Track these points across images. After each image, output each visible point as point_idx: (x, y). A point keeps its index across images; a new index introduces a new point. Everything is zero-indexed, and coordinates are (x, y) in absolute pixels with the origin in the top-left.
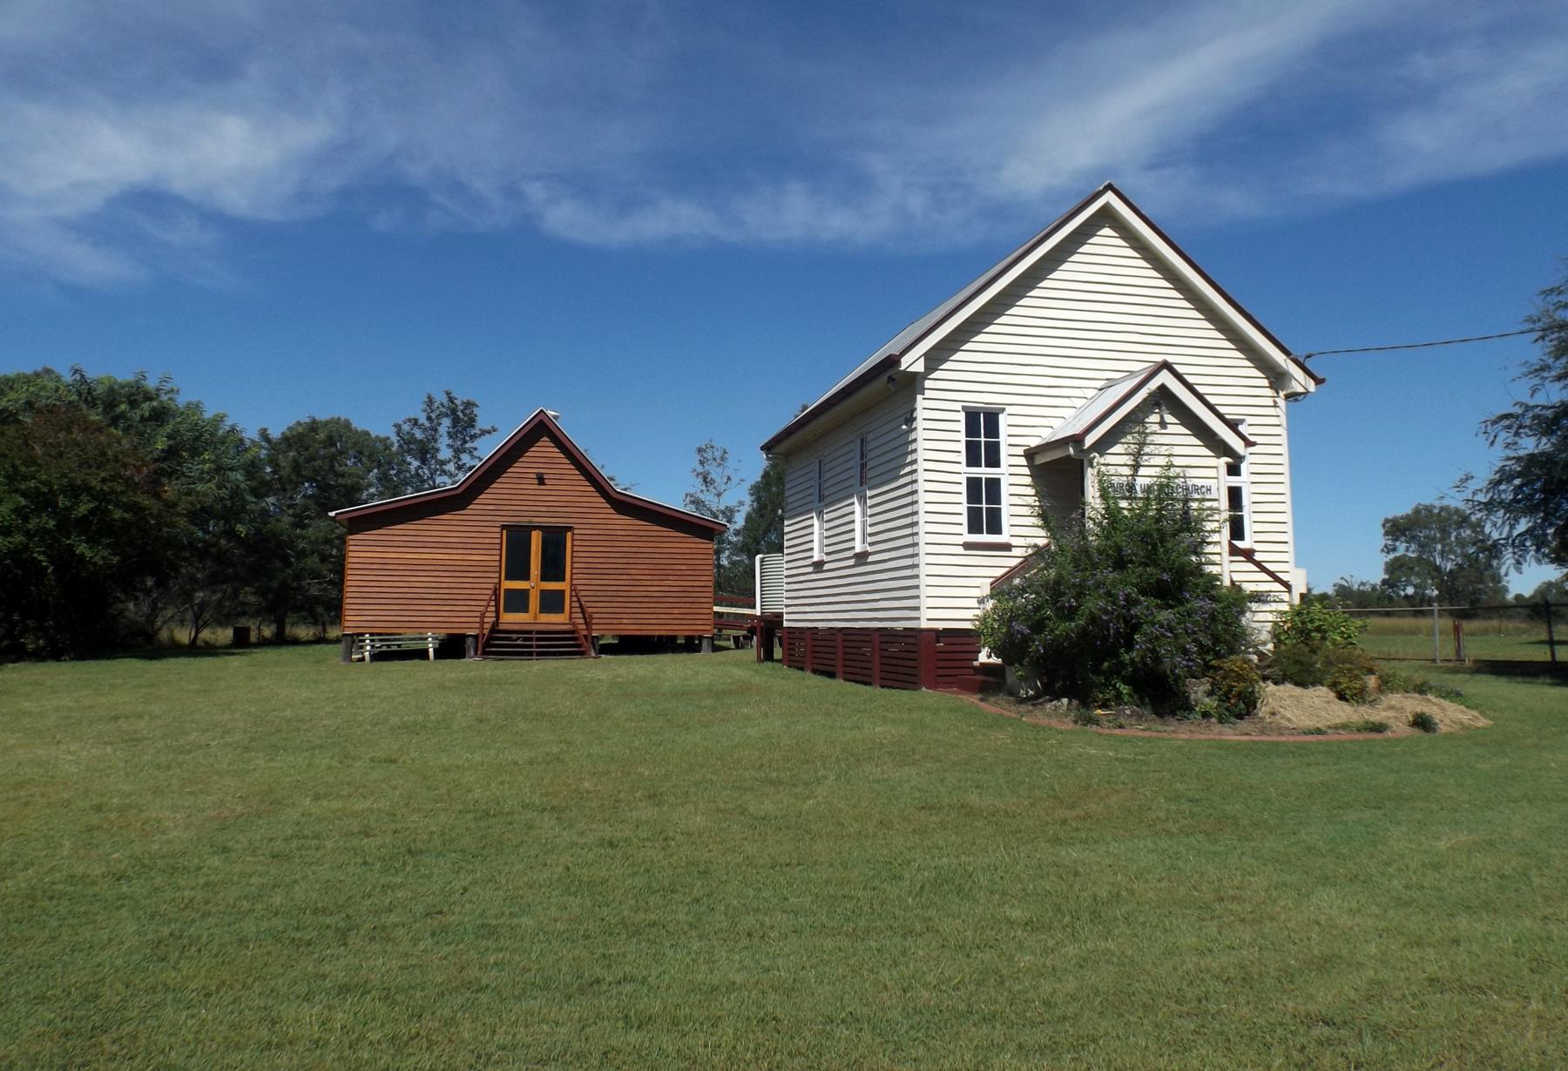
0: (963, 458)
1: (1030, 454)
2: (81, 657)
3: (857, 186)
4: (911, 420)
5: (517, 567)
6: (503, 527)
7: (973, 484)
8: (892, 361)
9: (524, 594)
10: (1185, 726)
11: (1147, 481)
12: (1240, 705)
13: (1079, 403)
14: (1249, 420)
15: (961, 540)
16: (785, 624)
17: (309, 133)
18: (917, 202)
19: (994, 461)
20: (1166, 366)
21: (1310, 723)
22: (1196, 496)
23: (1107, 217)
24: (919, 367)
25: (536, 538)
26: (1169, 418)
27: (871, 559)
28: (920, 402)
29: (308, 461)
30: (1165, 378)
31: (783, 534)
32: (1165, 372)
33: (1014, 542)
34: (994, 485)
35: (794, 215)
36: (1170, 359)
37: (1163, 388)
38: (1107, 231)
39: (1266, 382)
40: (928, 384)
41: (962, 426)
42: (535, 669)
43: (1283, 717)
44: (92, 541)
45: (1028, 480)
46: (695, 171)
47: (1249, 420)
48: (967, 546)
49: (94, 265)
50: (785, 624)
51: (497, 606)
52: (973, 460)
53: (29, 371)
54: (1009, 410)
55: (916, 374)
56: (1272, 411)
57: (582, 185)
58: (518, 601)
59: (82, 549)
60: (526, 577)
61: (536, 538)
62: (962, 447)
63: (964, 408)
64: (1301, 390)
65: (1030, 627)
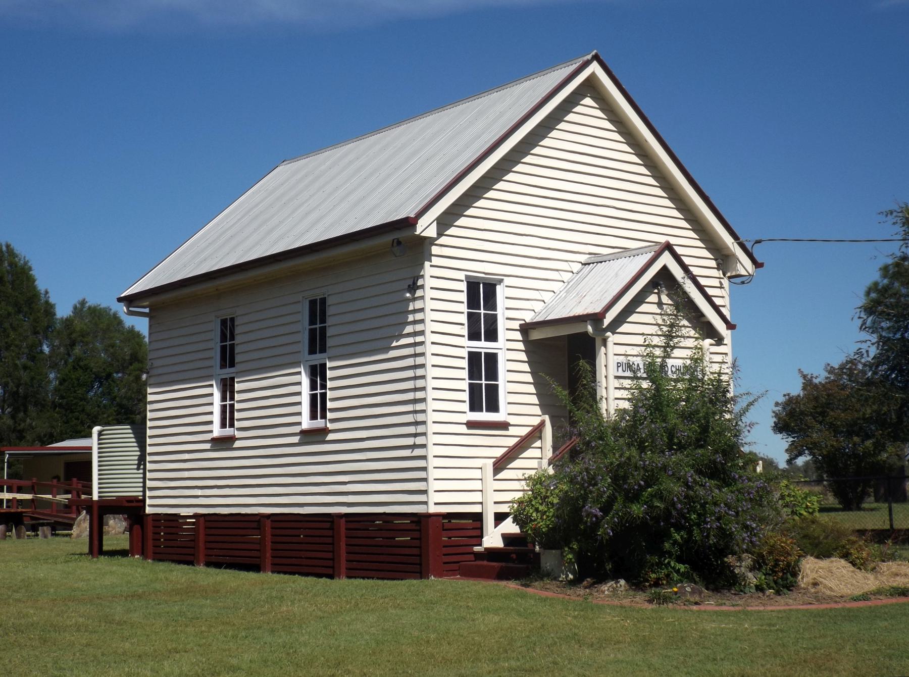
0: (465, 331)
1: (526, 329)
4: (414, 287)
7: (474, 358)
8: (409, 223)
10: (737, 600)
11: (679, 363)
12: (783, 578)
13: (566, 276)
15: (464, 418)
16: (148, 510)
19: (492, 335)
20: (668, 247)
21: (858, 592)
24: (432, 232)
27: (331, 437)
28: (428, 270)
31: (146, 403)
32: (667, 254)
33: (512, 420)
34: (492, 359)
36: (673, 241)
38: (588, 101)
39: (713, 264)
41: (463, 297)
42: (219, 578)
43: (825, 587)
45: (523, 357)
48: (471, 425)
50: (148, 510)
52: (474, 335)
54: (507, 281)
55: (425, 238)
62: (464, 319)
64: (744, 272)
65: (601, 510)
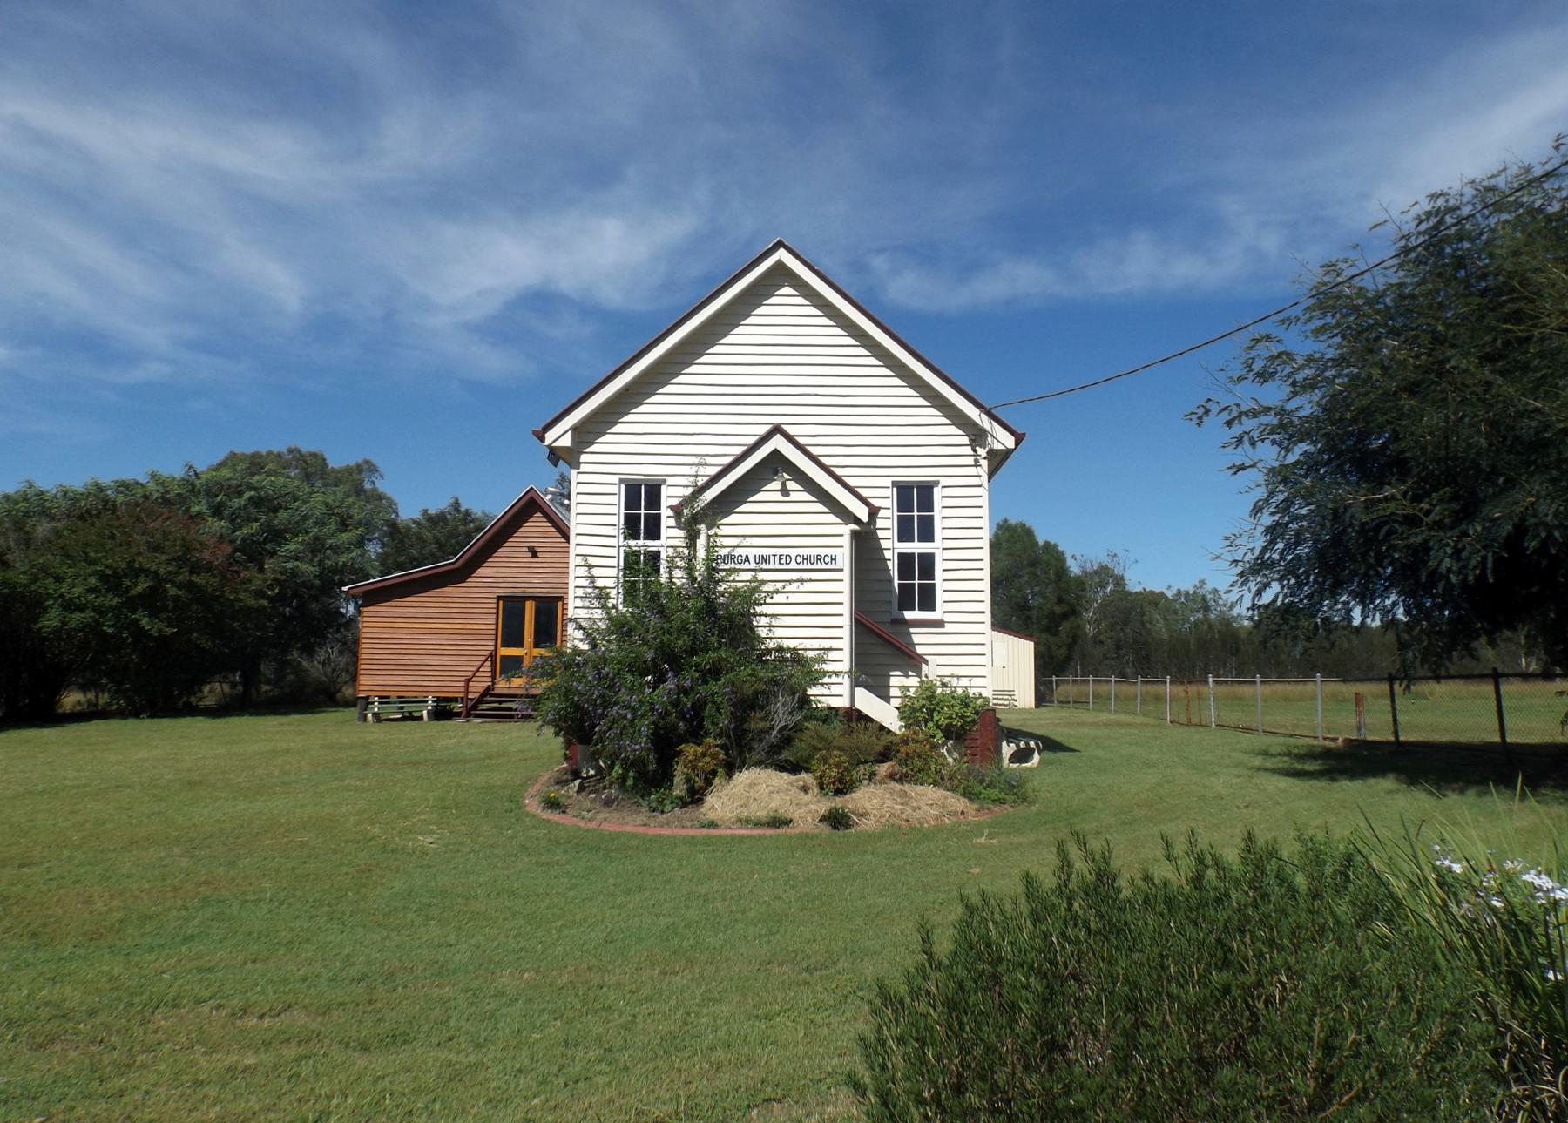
2: (153, 715)
3: (1205, 230)
5: (512, 636)
6: (499, 598)
9: (519, 659)
14: (944, 482)
17: (676, 227)
18: (1270, 243)
22: (723, 566)
23: (781, 275)
25: (530, 607)
26: (791, 485)
29: (448, 538)
30: (778, 443)
35: (1140, 266)
37: (776, 452)
38: (787, 290)
39: (966, 440)
40: (584, 458)
44: (154, 614)
46: (1031, 230)
47: (944, 482)
49: (495, 363)
51: (494, 671)
53: (352, 463)
54: (670, 481)
56: (973, 471)
57: (925, 254)
58: (511, 666)
59: (145, 622)
60: (521, 645)
61: (530, 607)
63: (621, 481)
